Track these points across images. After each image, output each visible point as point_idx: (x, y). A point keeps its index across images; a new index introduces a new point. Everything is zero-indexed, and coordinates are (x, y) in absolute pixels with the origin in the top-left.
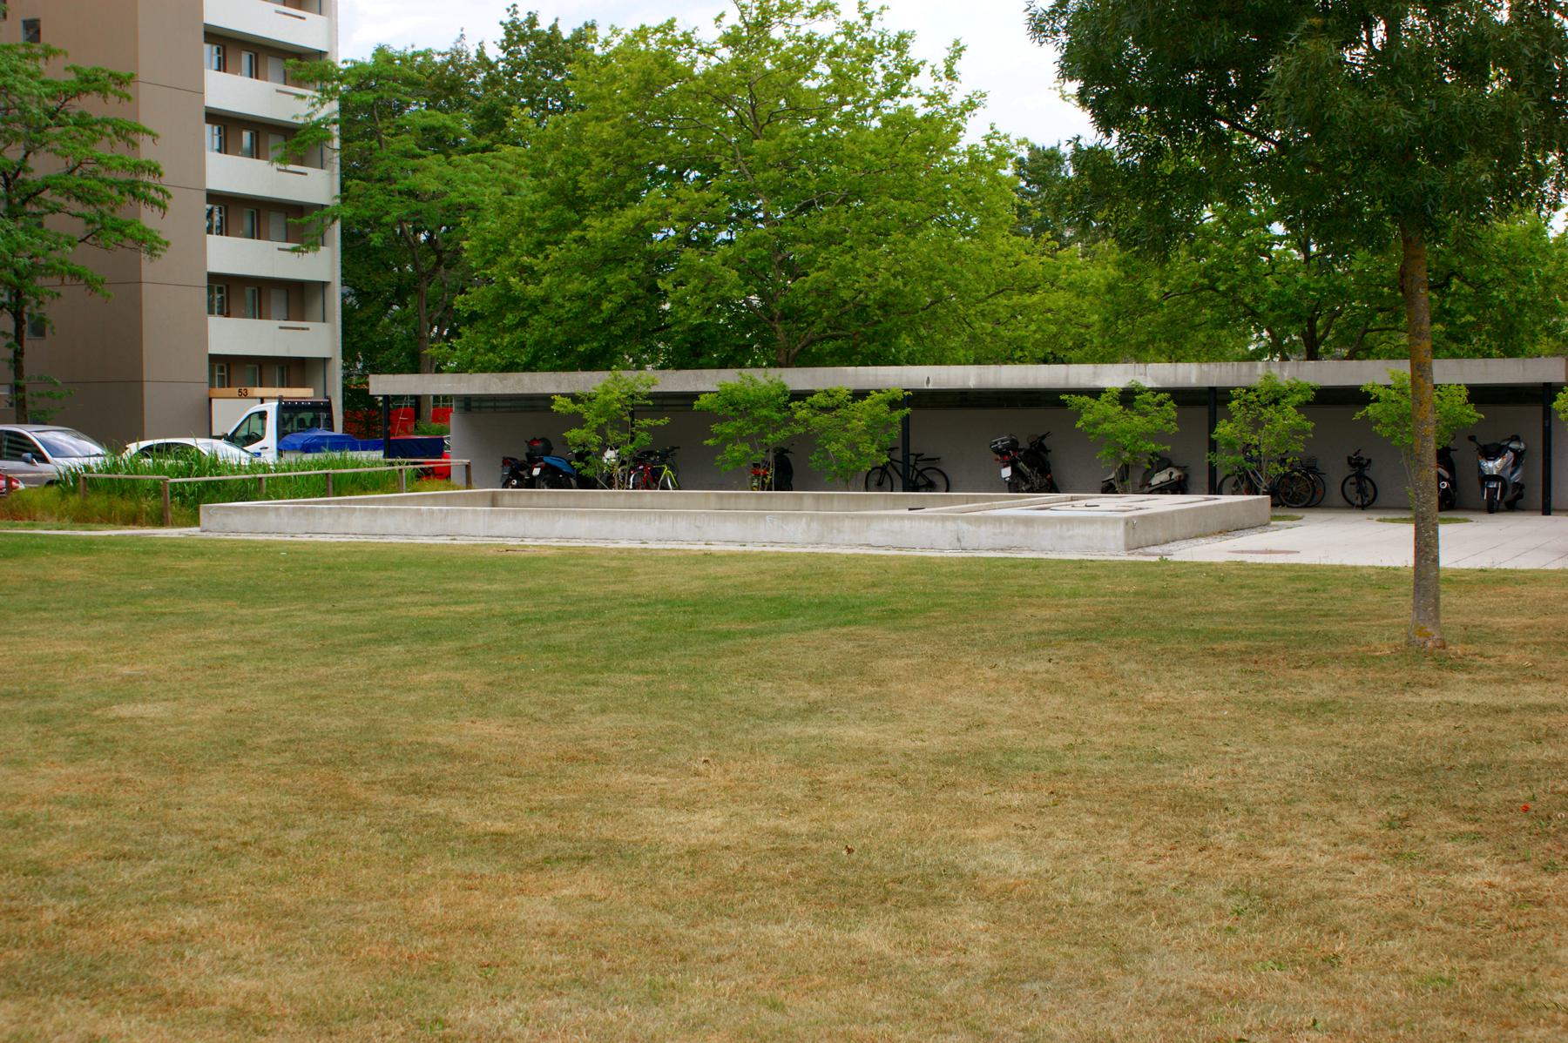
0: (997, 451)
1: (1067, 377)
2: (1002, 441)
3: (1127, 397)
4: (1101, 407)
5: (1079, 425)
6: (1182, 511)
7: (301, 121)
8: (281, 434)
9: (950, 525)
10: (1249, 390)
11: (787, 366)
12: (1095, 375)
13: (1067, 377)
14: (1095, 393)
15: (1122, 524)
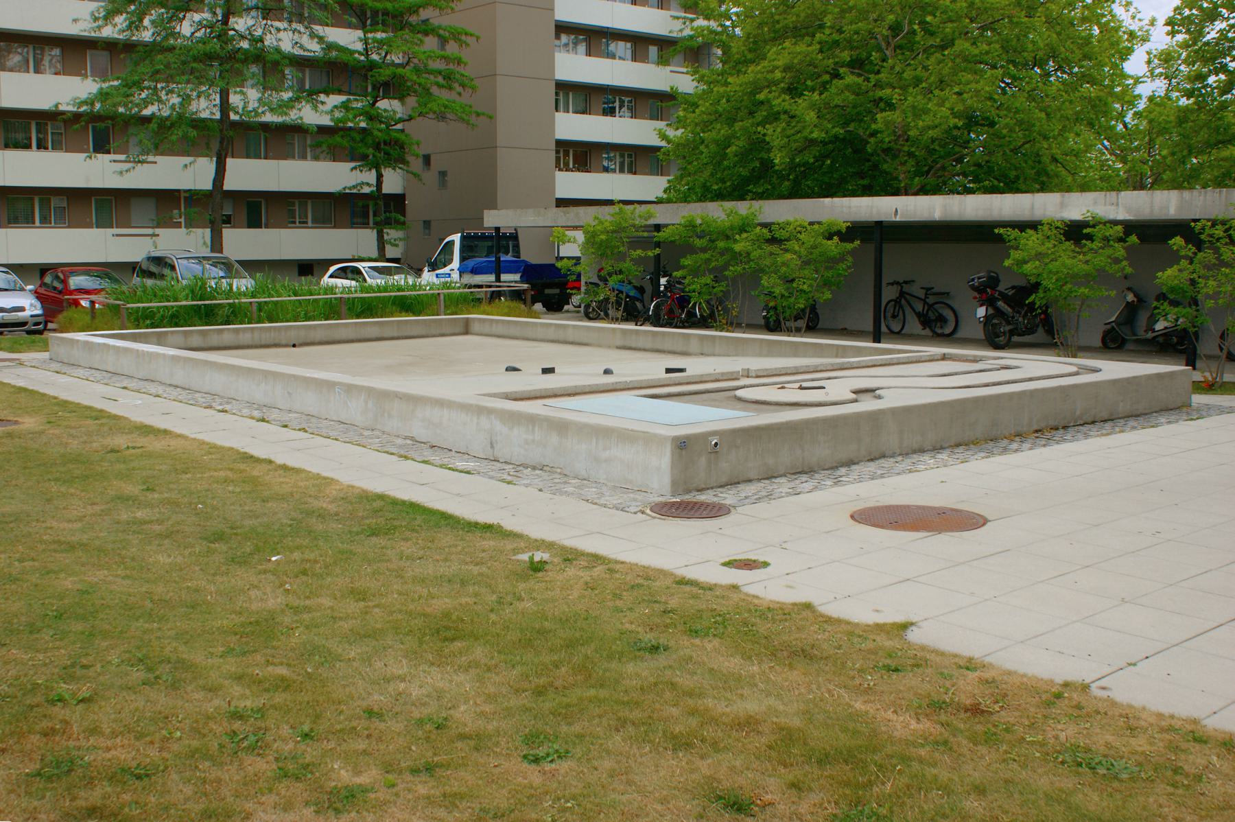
0: (973, 288)
1: (1032, 208)
2: (979, 277)
3: (1075, 232)
4: (1031, 240)
5: (1007, 263)
6: (977, 401)
7: (675, 35)
8: (463, 259)
9: (485, 422)
10: (1214, 223)
11: (768, 198)
12: (1062, 205)
13: (1032, 208)
14: (1034, 225)
15: (668, 450)
